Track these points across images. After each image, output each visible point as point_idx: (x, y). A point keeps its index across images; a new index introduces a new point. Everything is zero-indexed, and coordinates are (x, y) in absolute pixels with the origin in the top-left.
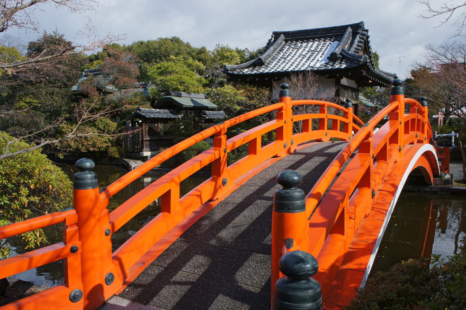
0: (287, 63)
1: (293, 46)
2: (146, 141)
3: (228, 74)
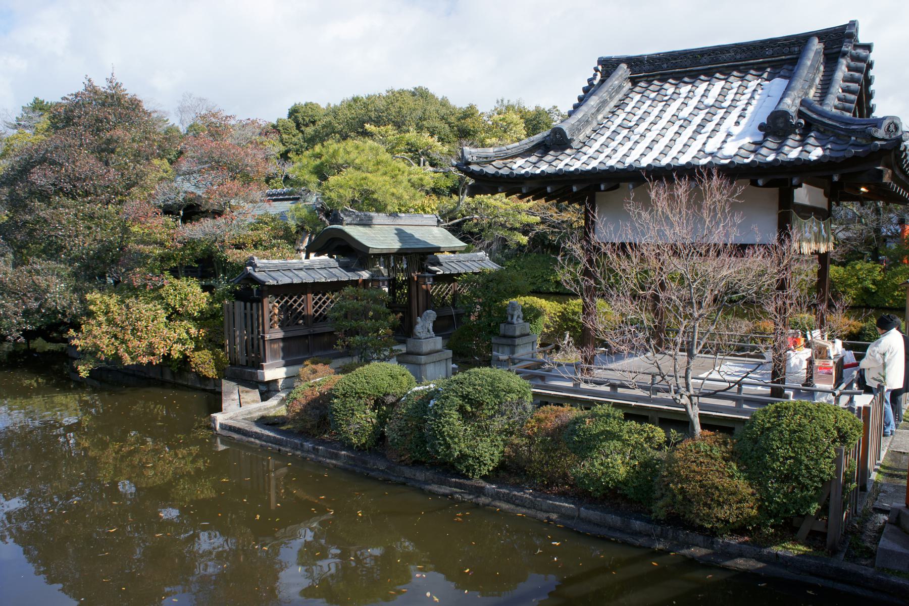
0: (637, 142)
1: (653, 95)
2: (272, 341)
3: (472, 174)
